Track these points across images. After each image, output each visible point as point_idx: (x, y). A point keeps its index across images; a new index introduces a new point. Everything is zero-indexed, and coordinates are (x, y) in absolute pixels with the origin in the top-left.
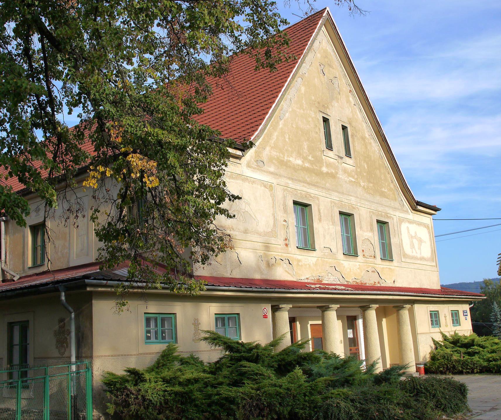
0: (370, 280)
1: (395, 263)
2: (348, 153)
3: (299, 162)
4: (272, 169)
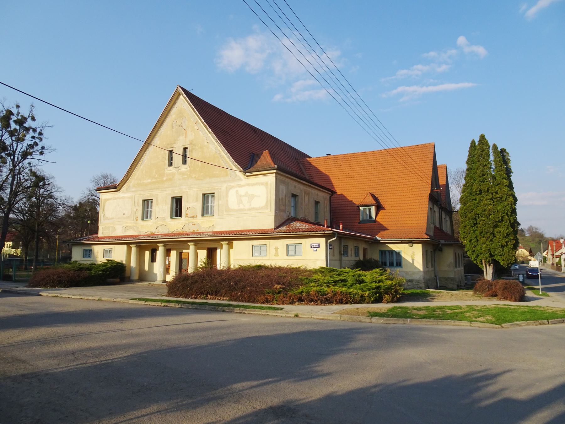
0: (187, 230)
1: (216, 217)
2: (184, 162)
3: (149, 181)
4: (133, 190)
